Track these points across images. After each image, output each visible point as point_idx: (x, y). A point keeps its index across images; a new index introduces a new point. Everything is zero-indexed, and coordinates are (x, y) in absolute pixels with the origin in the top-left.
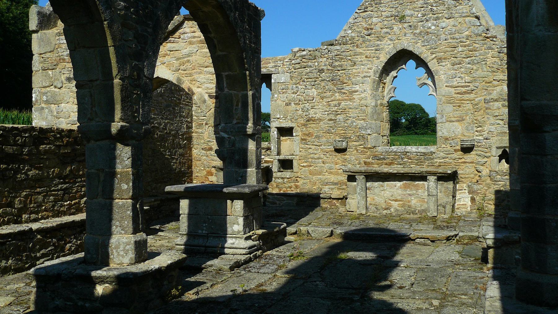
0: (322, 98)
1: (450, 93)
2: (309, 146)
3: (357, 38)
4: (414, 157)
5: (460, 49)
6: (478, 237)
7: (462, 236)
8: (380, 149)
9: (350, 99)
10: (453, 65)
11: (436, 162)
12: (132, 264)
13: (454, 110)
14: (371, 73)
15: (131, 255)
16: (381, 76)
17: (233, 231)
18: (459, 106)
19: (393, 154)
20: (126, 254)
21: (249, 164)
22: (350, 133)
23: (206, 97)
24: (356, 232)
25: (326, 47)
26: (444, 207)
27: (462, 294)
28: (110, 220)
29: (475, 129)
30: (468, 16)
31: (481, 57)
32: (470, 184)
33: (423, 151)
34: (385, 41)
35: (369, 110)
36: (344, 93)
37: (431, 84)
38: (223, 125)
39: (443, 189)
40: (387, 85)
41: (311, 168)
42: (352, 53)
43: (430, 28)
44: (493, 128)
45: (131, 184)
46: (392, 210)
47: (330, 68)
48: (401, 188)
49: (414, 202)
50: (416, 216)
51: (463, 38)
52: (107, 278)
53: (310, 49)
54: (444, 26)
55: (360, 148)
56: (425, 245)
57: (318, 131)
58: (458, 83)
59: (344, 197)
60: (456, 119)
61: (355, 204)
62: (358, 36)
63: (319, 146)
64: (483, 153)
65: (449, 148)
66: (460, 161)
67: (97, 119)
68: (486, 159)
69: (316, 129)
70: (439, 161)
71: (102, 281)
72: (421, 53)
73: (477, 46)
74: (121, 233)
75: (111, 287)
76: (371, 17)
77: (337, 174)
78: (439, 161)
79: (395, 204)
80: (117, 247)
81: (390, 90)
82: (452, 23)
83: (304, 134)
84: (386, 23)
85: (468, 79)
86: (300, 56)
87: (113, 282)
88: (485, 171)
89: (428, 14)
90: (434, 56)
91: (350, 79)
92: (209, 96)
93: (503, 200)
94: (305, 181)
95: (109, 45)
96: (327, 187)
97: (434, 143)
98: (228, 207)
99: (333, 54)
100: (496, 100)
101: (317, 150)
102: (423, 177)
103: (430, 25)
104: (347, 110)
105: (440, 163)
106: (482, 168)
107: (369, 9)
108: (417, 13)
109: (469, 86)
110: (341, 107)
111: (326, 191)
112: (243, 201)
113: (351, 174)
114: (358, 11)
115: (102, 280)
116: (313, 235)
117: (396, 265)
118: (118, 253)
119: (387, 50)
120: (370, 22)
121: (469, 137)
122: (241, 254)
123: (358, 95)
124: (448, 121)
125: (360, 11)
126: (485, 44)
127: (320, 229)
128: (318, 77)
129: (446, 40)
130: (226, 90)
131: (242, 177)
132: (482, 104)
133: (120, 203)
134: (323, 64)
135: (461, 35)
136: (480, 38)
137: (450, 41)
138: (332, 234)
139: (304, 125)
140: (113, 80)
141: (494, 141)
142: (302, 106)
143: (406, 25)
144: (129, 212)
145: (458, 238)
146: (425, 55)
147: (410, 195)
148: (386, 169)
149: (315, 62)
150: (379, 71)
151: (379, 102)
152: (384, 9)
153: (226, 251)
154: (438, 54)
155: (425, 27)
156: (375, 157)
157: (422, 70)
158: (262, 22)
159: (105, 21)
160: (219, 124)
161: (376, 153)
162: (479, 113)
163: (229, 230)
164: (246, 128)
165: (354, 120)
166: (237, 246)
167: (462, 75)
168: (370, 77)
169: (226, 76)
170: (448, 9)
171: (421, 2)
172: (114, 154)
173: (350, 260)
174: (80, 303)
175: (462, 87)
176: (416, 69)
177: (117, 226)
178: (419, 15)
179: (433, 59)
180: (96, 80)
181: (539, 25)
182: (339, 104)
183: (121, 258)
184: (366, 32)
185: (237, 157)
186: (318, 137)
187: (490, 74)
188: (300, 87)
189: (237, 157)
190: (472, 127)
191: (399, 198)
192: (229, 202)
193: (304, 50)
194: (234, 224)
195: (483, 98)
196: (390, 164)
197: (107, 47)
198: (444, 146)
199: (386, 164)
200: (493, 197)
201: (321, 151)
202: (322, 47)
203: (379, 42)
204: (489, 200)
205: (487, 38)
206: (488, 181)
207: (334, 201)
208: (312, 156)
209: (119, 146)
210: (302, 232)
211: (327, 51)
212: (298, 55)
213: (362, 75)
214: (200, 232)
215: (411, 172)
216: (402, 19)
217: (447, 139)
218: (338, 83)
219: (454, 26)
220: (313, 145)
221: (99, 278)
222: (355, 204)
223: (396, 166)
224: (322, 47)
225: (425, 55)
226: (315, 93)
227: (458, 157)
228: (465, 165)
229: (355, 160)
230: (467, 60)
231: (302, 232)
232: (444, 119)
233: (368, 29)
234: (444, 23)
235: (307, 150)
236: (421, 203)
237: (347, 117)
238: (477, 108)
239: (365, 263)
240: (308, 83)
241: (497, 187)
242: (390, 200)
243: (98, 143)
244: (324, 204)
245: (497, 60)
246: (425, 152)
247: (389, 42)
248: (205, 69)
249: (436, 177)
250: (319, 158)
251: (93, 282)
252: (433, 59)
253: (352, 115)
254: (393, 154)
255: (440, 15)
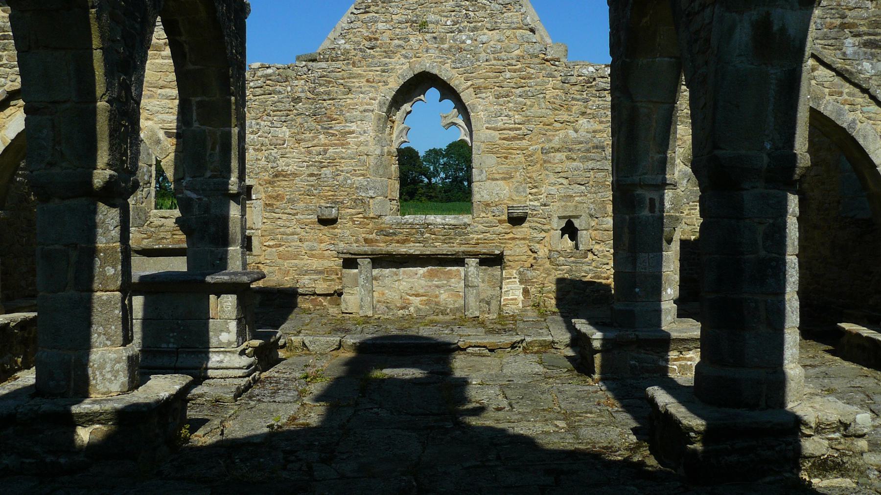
0: (298, 141)
1: (493, 137)
2: (277, 216)
3: (353, 52)
4: (439, 232)
5: (508, 75)
6: (553, 342)
7: (531, 342)
8: (387, 219)
9: (342, 145)
10: (498, 97)
11: (473, 239)
12: (123, 393)
13: (498, 163)
14: (375, 105)
15: (123, 378)
16: (389, 111)
17: (220, 342)
18: (506, 158)
19: (408, 226)
20: (116, 377)
21: (230, 240)
22: (341, 196)
23: (161, 135)
24: (378, 342)
25: (304, 63)
26: (488, 303)
27: (586, 413)
28: (89, 324)
29: (528, 191)
30: (520, 28)
31: (538, 88)
32: (522, 269)
33: (453, 222)
34: (396, 58)
35: (372, 161)
36: (333, 135)
37: (463, 124)
38: (188, 179)
39: (487, 278)
40: (396, 123)
41: (281, 249)
42: (345, 74)
43: (464, 42)
44: (553, 190)
45: (120, 267)
46: (412, 309)
47: (310, 95)
48: (424, 277)
49: (444, 296)
50: (447, 318)
51: (512, 59)
52: (101, 414)
53: (279, 66)
54: (484, 41)
55: (358, 218)
56: (481, 355)
57: (292, 192)
58: (504, 124)
59: (335, 291)
60: (502, 176)
61: (353, 301)
62: (355, 49)
63: (294, 215)
64: (539, 225)
65: (491, 218)
66: (507, 236)
67: (64, 165)
68: (543, 234)
69: (288, 189)
70: (476, 236)
71: (89, 421)
72: (450, 79)
73: (532, 71)
74: (105, 345)
75: (105, 428)
76: (376, 22)
77: (322, 257)
78: (476, 236)
79: (416, 301)
80: (101, 367)
81: (401, 131)
82: (497, 37)
83: (269, 196)
84: (398, 31)
85: (518, 118)
86: (262, 76)
87: (111, 420)
88: (543, 252)
89: (462, 22)
90: (469, 83)
91: (342, 114)
92: (166, 133)
93: (569, 292)
94: (271, 269)
95: (94, 47)
96: (306, 277)
97: (468, 210)
98: (211, 305)
99: (316, 75)
100: (558, 150)
101: (290, 221)
102: (458, 261)
103: (464, 38)
104: (337, 160)
105: (478, 239)
106: (538, 246)
107: (372, 8)
108: (445, 19)
109: (520, 129)
110: (327, 155)
111: (305, 283)
112: (235, 296)
113: (350, 256)
114: (355, 11)
115: (89, 419)
116: (311, 348)
117: (464, 383)
118: (104, 376)
119: (399, 72)
120: (373, 29)
121: (520, 202)
122: (235, 377)
123: (354, 137)
124: (489, 179)
125: (359, 12)
126: (544, 69)
127: (323, 339)
128: (292, 108)
129: (487, 61)
130: (196, 125)
131: (220, 259)
132: (539, 155)
133: (105, 298)
134: (300, 90)
135: (509, 55)
136: (537, 61)
137: (494, 62)
138: (340, 346)
139: (270, 183)
140: (96, 102)
141: (555, 208)
142: (266, 153)
143: (428, 36)
144: (117, 312)
145: (524, 344)
146: (457, 81)
147: (438, 287)
148: (403, 249)
149: (286, 86)
150: (387, 103)
151: (386, 149)
152: (396, 10)
153: (210, 373)
154: (475, 81)
155: (456, 40)
156: (381, 231)
157: (449, 103)
158: (249, 22)
159: (92, 8)
160: (183, 178)
161: (383, 226)
162: (534, 168)
163: (213, 341)
164: (228, 184)
165: (349, 175)
166: (229, 365)
167: (510, 113)
168: (373, 111)
169: (198, 103)
170: (492, 15)
171: (452, 3)
172: (95, 220)
173: (392, 380)
174: (49, 459)
175: (510, 129)
176: (440, 101)
177: (99, 334)
178: (449, 23)
179: (468, 88)
180: (65, 102)
181: (740, 55)
182: (325, 152)
183: (107, 383)
184: (367, 44)
185: (212, 229)
186: (291, 201)
187: (550, 112)
188: (262, 123)
189: (212, 229)
190: (524, 188)
191: (421, 291)
192: (212, 297)
193: (269, 67)
194: (222, 331)
195: (539, 146)
196: (404, 242)
197: (90, 49)
198: (484, 215)
199: (398, 242)
200: (553, 287)
201: (297, 224)
202: (297, 63)
203: (387, 60)
204: (549, 292)
205: (547, 60)
206: (548, 265)
207: (320, 298)
208: (282, 230)
209: (102, 207)
210: (295, 344)
211: (305, 69)
212: (259, 73)
213: (361, 109)
214: (164, 345)
215: (441, 252)
216: (423, 27)
217: (488, 205)
218: (323, 119)
219: (499, 41)
220: (283, 213)
221: (87, 415)
222: (353, 301)
223: (412, 244)
224: (297, 63)
225: (457, 82)
226: (288, 134)
227: (504, 231)
228: (514, 242)
229: (350, 235)
230: (518, 91)
231: (295, 344)
232: (484, 176)
233: (370, 39)
234: (485, 36)
235: (274, 220)
236: (456, 299)
237: (338, 170)
238: (531, 161)
239: (414, 382)
240: (275, 118)
241: (559, 274)
242: (408, 294)
243: (67, 202)
244: (303, 303)
245: (560, 92)
246: (456, 223)
247: (403, 60)
248: (159, 91)
249: (478, 260)
250: (293, 234)
251: (71, 422)
252: (468, 88)
253: (345, 168)
254: (408, 226)
255: (480, 24)
